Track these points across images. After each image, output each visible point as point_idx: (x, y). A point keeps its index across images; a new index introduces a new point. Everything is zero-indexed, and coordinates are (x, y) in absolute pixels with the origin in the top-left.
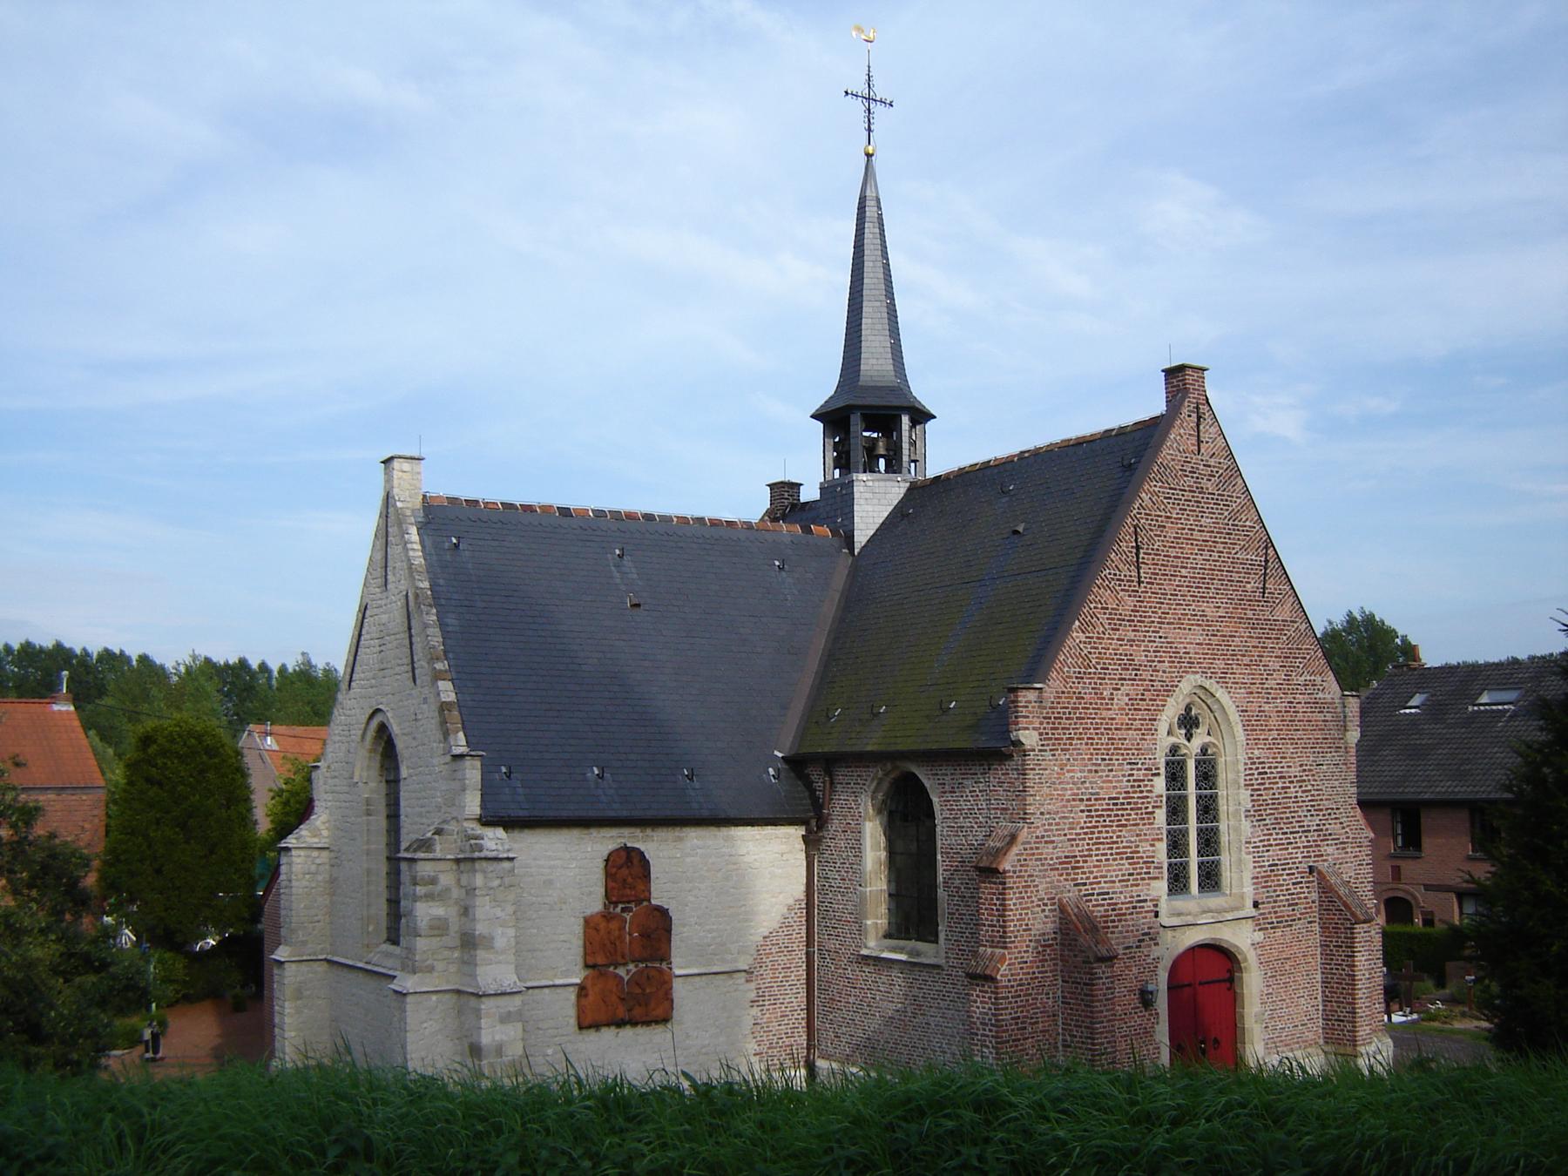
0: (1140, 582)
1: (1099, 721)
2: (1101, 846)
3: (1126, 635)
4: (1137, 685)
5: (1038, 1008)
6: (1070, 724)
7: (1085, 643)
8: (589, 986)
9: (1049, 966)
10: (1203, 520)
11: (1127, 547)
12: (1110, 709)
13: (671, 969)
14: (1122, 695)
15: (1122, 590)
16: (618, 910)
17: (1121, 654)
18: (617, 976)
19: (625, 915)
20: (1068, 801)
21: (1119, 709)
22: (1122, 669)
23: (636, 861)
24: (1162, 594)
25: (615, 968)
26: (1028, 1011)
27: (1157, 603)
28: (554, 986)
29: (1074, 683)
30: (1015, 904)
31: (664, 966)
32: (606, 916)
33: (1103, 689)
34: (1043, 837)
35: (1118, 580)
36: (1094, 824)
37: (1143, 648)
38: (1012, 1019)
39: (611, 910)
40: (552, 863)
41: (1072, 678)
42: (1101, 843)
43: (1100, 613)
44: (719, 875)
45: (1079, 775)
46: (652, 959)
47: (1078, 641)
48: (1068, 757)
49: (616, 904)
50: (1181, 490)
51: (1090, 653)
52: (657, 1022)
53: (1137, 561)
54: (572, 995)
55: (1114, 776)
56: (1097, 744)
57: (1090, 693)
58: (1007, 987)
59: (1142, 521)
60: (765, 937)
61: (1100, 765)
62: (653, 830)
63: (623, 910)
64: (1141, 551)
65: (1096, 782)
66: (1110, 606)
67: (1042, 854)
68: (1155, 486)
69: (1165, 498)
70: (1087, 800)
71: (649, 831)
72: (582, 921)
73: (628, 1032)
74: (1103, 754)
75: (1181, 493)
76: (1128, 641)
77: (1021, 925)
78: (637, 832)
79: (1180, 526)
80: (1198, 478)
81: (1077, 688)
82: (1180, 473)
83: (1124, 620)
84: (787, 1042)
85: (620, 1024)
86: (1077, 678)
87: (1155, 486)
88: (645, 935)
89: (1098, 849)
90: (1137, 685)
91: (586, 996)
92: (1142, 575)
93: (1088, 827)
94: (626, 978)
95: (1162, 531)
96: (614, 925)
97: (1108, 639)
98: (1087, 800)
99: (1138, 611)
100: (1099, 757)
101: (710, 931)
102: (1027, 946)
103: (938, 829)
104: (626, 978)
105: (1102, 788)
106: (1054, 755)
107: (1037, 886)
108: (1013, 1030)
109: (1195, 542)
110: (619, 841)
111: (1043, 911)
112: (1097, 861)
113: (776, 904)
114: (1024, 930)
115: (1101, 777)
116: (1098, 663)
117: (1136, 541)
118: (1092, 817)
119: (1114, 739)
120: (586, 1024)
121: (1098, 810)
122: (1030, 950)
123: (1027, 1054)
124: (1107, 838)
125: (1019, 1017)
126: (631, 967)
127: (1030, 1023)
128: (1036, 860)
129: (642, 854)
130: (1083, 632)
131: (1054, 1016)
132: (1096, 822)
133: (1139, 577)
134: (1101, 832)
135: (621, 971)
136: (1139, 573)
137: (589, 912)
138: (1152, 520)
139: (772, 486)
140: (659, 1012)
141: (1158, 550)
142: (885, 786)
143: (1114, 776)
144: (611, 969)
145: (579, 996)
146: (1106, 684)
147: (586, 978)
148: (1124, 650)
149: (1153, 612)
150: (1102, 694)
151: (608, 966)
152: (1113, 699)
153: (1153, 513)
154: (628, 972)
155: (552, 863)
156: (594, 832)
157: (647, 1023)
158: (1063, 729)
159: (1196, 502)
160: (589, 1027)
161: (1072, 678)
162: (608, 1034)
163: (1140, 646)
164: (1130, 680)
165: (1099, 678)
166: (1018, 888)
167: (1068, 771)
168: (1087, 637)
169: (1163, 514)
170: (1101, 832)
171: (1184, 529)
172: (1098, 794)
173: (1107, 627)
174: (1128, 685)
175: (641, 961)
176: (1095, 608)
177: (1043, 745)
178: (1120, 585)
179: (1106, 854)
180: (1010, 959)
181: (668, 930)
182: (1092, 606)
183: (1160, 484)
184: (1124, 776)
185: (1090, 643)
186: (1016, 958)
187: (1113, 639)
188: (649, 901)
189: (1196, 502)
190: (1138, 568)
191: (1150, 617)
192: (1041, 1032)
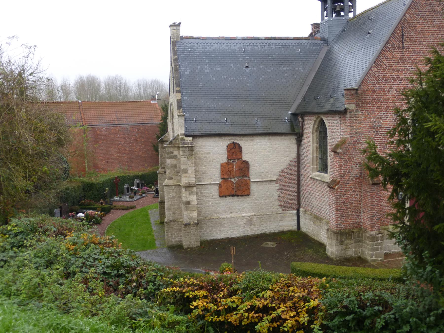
0: (403, 48)
1: (383, 100)
2: (382, 144)
3: (396, 68)
4: (401, 86)
5: (353, 199)
6: (370, 101)
7: (377, 72)
8: (222, 184)
9: (357, 185)
10: (434, 23)
11: (398, 35)
12: (388, 96)
13: (249, 179)
14: (393, 90)
15: (395, 52)
16: (231, 161)
17: (394, 75)
18: (231, 181)
19: (234, 163)
20: (368, 129)
21: (392, 95)
22: (394, 81)
23: (237, 147)
24: (413, 52)
25: (231, 179)
26: (348, 200)
27: (411, 55)
28: (211, 184)
29: (372, 86)
30: (344, 164)
31: (247, 178)
32: (228, 164)
33: (385, 88)
34: (356, 141)
35: (393, 48)
36: (379, 136)
37: (403, 73)
38: (342, 202)
39: (229, 161)
40: (210, 147)
41: (371, 85)
42: (382, 143)
43: (384, 61)
44: (266, 151)
45: (373, 119)
46: (243, 176)
47: (374, 71)
48: (368, 113)
49: (230, 160)
50: (424, 12)
51: (379, 75)
52: (245, 195)
53: (402, 40)
54: (217, 187)
55: (388, 119)
56: (381, 108)
57: (379, 90)
58: (340, 192)
59: (405, 25)
60: (282, 170)
61: (382, 116)
62: (243, 137)
63: (233, 162)
64: (405, 36)
65: (380, 122)
66: (389, 58)
67: (356, 147)
68: (412, 11)
69: (417, 15)
70: (376, 128)
71: (241, 138)
72: (220, 165)
73: (236, 198)
74: (384, 112)
75: (424, 13)
76: (397, 70)
77: (346, 171)
78: (238, 138)
79: (423, 26)
80: (433, 6)
81: (373, 88)
82: (424, 5)
83: (395, 63)
84: (290, 202)
85: (233, 196)
86: (373, 85)
87: (412, 11)
88: (240, 169)
89: (381, 145)
90: (401, 86)
91: (221, 187)
92: (405, 45)
93: (376, 138)
94: (234, 182)
95: (415, 28)
96: (230, 166)
97: (388, 70)
98: (376, 128)
99: (402, 59)
100: (382, 113)
101: (263, 168)
102: (349, 178)
103: (328, 137)
104: (234, 182)
105: (383, 124)
106: (362, 113)
107: (354, 158)
108: (342, 206)
109: (430, 31)
110: (231, 141)
111: (356, 166)
112: (380, 149)
113: (286, 160)
114: (348, 173)
115: (383, 120)
116: (383, 79)
117: (402, 32)
118: (378, 134)
119: (389, 106)
120: (222, 195)
121: (381, 132)
122: (350, 180)
123: (348, 214)
124: (384, 141)
125: (345, 202)
126: (236, 179)
127: (349, 204)
128: (354, 149)
129: (239, 145)
130: (376, 68)
131: (360, 202)
132: (380, 136)
133: (403, 46)
134: (382, 139)
135: (233, 180)
136: (403, 45)
137: (222, 162)
138: (410, 24)
139: (312, 25)
140: (246, 193)
141: (412, 35)
142: (317, 123)
143: (388, 119)
144: (229, 179)
145: (219, 187)
146: (386, 86)
147: (221, 182)
148: (395, 74)
149: (409, 59)
150: (384, 90)
151: (229, 178)
152: (389, 92)
153: (411, 21)
154: (235, 180)
155: (210, 147)
156: (223, 138)
157: (242, 196)
158: (366, 103)
159: (431, 16)
160: (223, 196)
161: (371, 85)
162: (228, 199)
163: (403, 72)
164: (397, 84)
165: (383, 85)
166: (345, 159)
167: (368, 118)
168: (378, 70)
169: (416, 21)
170: (382, 139)
171: (425, 27)
172: (381, 126)
173: (387, 65)
174: (396, 86)
175: (240, 177)
176: (382, 59)
177: (357, 109)
178: (394, 50)
179: (384, 147)
180: (342, 182)
181: (248, 168)
182: (381, 58)
183: (415, 10)
184: (393, 119)
185: (379, 72)
186: (344, 182)
187: (390, 70)
188: (242, 159)
189: (431, 16)
190: (403, 43)
191: (407, 61)
192: (354, 207)
